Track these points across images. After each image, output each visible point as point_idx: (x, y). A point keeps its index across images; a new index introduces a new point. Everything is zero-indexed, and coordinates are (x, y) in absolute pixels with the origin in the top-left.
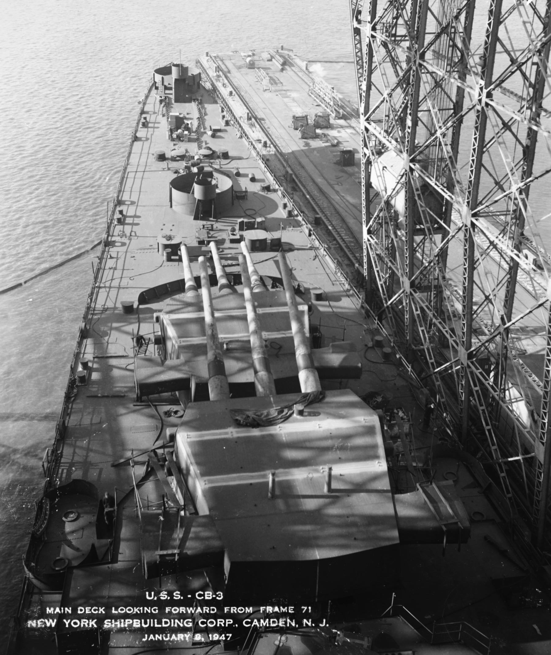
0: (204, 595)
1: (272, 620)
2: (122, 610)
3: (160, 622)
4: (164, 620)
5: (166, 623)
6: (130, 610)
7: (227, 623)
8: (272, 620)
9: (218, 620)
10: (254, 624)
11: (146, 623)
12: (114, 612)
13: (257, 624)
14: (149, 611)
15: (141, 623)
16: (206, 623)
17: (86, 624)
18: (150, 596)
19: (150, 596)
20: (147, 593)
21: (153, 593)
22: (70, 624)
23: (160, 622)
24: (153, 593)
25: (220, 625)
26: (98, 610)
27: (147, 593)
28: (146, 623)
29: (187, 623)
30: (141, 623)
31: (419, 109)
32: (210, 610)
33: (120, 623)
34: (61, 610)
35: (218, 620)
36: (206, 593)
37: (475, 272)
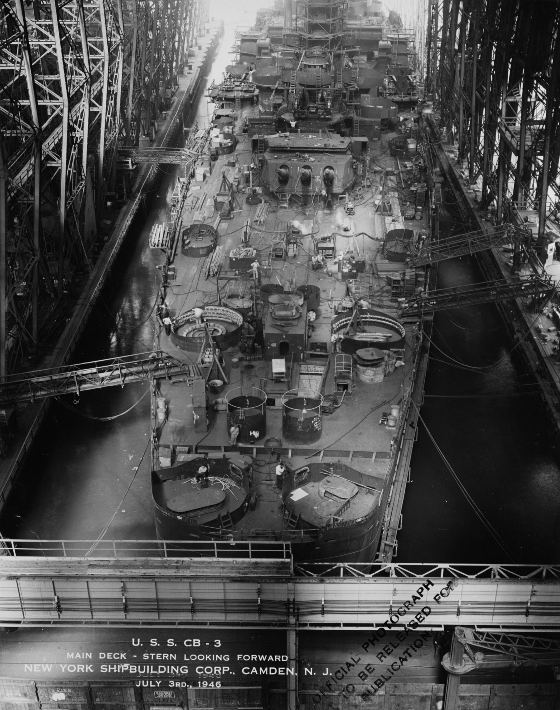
0: (192, 643)
1: (271, 668)
2: (193, 657)
3: (156, 669)
4: (160, 667)
5: (162, 669)
6: (201, 657)
7: (224, 670)
8: (271, 668)
9: (79, 666)
10: (253, 671)
11: (142, 670)
12: (185, 659)
13: (256, 671)
14: (221, 659)
15: (137, 669)
16: (203, 670)
17: (82, 669)
18: (136, 643)
19: (136, 643)
20: (133, 640)
21: (139, 640)
22: (66, 668)
23: (156, 669)
24: (139, 640)
25: (217, 672)
26: (120, 656)
27: (133, 640)
28: (142, 670)
29: (183, 669)
30: (137, 669)
31: (215, 228)
32: (281, 659)
33: (121, 670)
34: (81, 656)
35: (79, 666)
36: (194, 640)
37: (211, 254)
